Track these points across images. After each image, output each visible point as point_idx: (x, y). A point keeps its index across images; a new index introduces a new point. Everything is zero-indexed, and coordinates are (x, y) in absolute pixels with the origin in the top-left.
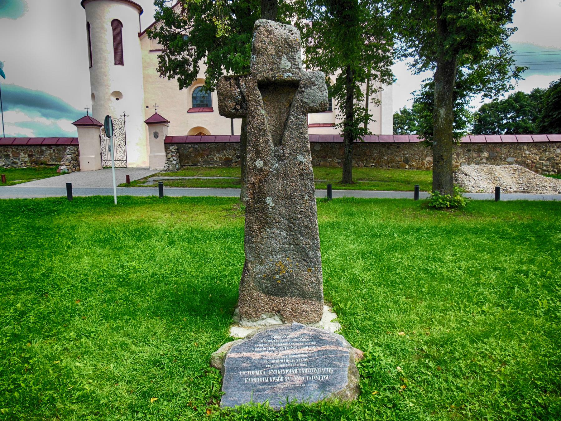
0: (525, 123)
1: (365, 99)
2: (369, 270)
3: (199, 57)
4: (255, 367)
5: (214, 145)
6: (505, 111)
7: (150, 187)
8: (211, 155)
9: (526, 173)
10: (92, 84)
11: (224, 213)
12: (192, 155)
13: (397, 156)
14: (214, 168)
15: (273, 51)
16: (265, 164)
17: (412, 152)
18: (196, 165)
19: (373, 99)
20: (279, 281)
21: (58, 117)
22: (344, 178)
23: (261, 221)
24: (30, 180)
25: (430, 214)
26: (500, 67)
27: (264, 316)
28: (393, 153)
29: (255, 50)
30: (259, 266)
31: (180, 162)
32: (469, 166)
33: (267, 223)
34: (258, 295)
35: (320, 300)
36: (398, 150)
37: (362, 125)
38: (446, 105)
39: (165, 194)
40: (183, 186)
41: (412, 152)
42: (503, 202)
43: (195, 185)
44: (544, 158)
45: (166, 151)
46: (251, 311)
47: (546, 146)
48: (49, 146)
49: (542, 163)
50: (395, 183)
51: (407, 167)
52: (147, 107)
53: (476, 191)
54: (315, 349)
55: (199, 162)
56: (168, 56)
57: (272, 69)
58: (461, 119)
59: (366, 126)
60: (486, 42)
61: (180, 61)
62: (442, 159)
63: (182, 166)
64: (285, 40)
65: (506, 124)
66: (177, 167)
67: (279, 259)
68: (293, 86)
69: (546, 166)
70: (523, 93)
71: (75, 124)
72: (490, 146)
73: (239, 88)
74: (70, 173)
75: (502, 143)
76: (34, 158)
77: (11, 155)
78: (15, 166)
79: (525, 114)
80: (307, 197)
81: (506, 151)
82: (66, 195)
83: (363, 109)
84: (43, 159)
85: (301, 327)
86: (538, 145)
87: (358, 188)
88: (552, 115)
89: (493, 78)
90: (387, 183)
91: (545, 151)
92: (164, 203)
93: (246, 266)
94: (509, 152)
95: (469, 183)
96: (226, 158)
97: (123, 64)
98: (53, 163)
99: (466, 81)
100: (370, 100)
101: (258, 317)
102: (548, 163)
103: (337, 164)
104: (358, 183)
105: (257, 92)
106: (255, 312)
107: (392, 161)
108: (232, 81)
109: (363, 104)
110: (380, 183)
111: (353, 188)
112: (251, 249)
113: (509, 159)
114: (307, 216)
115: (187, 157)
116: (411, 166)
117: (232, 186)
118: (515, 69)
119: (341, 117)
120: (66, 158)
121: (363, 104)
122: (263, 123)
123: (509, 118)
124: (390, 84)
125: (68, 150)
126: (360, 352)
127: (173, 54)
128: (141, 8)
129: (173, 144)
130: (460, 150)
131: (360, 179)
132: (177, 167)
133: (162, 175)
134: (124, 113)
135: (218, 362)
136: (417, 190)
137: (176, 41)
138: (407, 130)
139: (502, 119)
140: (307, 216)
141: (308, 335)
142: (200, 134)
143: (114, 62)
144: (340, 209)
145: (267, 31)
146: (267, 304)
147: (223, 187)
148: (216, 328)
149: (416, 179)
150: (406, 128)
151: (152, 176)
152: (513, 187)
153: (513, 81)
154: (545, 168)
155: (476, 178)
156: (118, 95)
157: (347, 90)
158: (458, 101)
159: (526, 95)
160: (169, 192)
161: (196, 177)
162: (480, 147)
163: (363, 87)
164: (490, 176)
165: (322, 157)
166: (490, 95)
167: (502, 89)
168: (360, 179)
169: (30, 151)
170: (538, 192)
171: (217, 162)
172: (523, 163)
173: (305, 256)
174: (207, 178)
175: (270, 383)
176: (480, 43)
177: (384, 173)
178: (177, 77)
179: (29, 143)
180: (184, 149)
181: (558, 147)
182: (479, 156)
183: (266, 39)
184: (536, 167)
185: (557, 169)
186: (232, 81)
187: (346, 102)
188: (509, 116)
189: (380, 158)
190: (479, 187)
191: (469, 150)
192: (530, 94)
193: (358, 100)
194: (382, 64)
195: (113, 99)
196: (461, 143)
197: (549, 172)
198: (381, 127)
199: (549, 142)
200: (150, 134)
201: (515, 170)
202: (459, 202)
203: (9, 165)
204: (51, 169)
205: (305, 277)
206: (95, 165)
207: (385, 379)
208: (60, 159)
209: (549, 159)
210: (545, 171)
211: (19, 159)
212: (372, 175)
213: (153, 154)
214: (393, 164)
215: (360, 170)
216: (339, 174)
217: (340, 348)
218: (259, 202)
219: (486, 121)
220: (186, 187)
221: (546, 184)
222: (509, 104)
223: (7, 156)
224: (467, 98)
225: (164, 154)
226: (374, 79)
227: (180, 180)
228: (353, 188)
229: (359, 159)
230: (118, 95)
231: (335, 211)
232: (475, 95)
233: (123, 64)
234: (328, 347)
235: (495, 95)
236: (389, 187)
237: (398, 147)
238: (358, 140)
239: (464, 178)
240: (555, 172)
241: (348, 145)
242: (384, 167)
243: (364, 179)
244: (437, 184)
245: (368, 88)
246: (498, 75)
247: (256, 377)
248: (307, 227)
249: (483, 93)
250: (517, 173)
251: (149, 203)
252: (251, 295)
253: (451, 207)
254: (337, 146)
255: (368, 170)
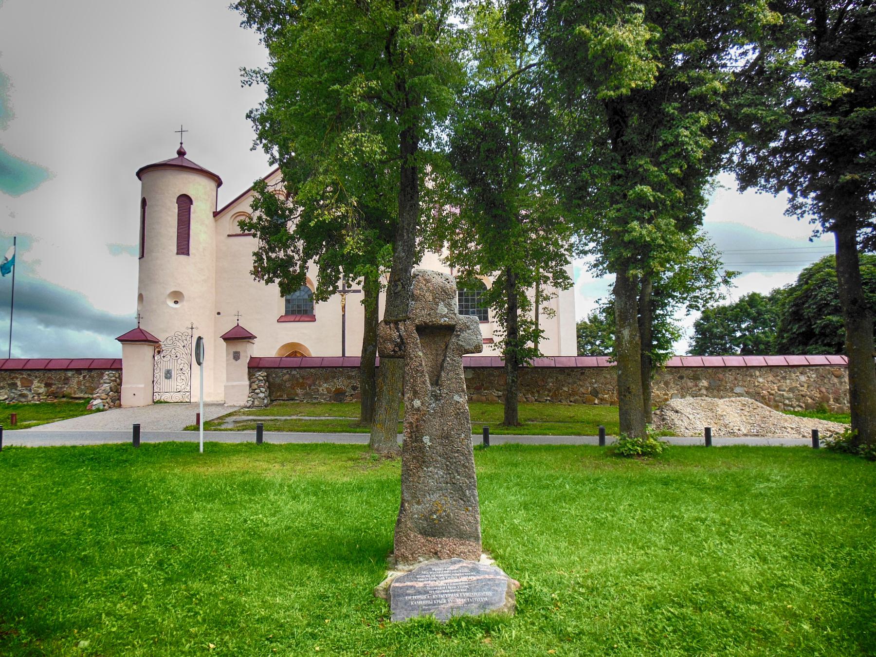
0: (767, 337)
1: (534, 309)
2: (531, 520)
3: (308, 255)
4: (420, 593)
5: (320, 371)
6: (738, 320)
7: (231, 430)
8: (315, 384)
9: (759, 409)
10: (141, 281)
11: (350, 463)
12: (288, 385)
13: (582, 386)
14: (320, 403)
15: (431, 298)
16: (422, 404)
17: (603, 380)
18: (293, 399)
19: (544, 309)
20: (436, 522)
21: (64, 325)
22: (506, 418)
23: (418, 460)
24: (48, 420)
25: (616, 464)
26: (706, 272)
27: (421, 559)
28: (575, 382)
29: (414, 297)
30: (416, 506)
31: (270, 395)
32: (682, 400)
33: (424, 462)
34: (415, 536)
35: (478, 540)
36: (582, 377)
37: (530, 344)
38: (629, 325)
39: (264, 440)
40: (279, 430)
41: (603, 380)
42: (715, 447)
43: (296, 428)
44: (784, 388)
45: (250, 379)
46: (407, 554)
47: (785, 372)
48: (78, 371)
49: (783, 395)
50: (579, 424)
51: (596, 402)
52: (219, 313)
53: (691, 434)
54: (475, 578)
55: (297, 395)
56: (267, 253)
57: (429, 314)
58: (664, 335)
59: (536, 346)
60: (660, 258)
61: (282, 259)
62: (630, 393)
63: (272, 401)
64: (442, 288)
65: (740, 337)
66: (266, 401)
67: (437, 501)
68: (450, 329)
69: (788, 399)
70: (759, 295)
71: (120, 339)
72: (710, 371)
73: (398, 331)
74: (106, 410)
75: (726, 367)
76: (54, 388)
77: (19, 383)
78: (23, 400)
79: (764, 324)
80: (463, 435)
81: (732, 378)
82: (132, 441)
83: (531, 323)
84: (66, 390)
85: (460, 561)
86: (775, 370)
87: (527, 431)
88: (792, 328)
89: (698, 284)
90: (567, 425)
91: (784, 378)
92: (266, 452)
93: (402, 505)
94: (736, 379)
95: (681, 423)
96: (337, 390)
97: (188, 254)
98: (82, 395)
99: (666, 286)
100: (541, 311)
101: (415, 559)
102: (791, 395)
103: (497, 399)
104: (527, 425)
105: (416, 335)
106: (412, 554)
107: (574, 393)
108: (392, 325)
109: (530, 316)
110: (557, 424)
111: (519, 432)
112: (408, 488)
113: (738, 390)
114: (463, 455)
115: (280, 387)
116: (602, 400)
117: (348, 429)
118: (724, 274)
119: (501, 333)
120: (103, 388)
121: (530, 316)
122: (421, 365)
123: (745, 329)
124: (566, 288)
125: (106, 377)
126: (517, 582)
127: (273, 251)
128: (219, 179)
129: (260, 369)
130: (668, 377)
131: (529, 420)
132: (266, 401)
133: (244, 414)
134: (192, 324)
135: (382, 593)
136: (602, 434)
137: (279, 235)
138: (599, 346)
139: (735, 331)
140: (463, 455)
141: (467, 567)
142: (294, 354)
143: (175, 251)
144: (500, 458)
145: (425, 280)
146: (424, 546)
147: (335, 432)
148: (372, 572)
149: (608, 418)
150: (598, 343)
151: (230, 415)
152: (742, 429)
153: (723, 289)
154: (787, 402)
155: (691, 417)
156: (177, 297)
157: (509, 299)
158: (658, 312)
159: (763, 298)
160: (270, 437)
161: (294, 417)
162: (695, 373)
163: (530, 293)
164: (710, 414)
165: (475, 388)
166: (696, 306)
167: (710, 298)
168: (529, 420)
169: (49, 378)
170: (776, 435)
171: (324, 395)
172: (757, 396)
173: (461, 494)
174: (312, 418)
175: (434, 605)
176: (654, 258)
177: (564, 411)
178: (277, 280)
179: (49, 367)
180: (277, 376)
181: (801, 373)
182: (697, 386)
183: (424, 287)
184: (775, 401)
185: (804, 403)
186: (392, 325)
187: (507, 314)
188: (743, 326)
189: (558, 389)
190: (695, 429)
191: (681, 378)
192: (769, 296)
193: (523, 310)
194: (554, 263)
195: (171, 303)
196: (666, 367)
197: (794, 407)
198: (558, 343)
199: (789, 366)
200: (228, 355)
201: (744, 405)
202: (653, 447)
203: (14, 398)
204: (77, 404)
205: (463, 516)
206: (143, 399)
207: (540, 601)
208: (92, 390)
209: (791, 390)
210: (789, 405)
211: (30, 390)
212: (547, 413)
213: (230, 384)
214: (577, 397)
215: (529, 407)
216: (499, 412)
217: (498, 577)
218: (416, 441)
219: (712, 333)
220: (283, 431)
221: (786, 425)
222: (741, 310)
223: (14, 386)
224: (669, 309)
225: (248, 383)
226: (545, 282)
227: (272, 420)
228: (519, 432)
229: (528, 391)
230: (177, 297)
231: (494, 461)
232: (680, 305)
233: (188, 254)
234: (487, 576)
235: (703, 306)
236: (570, 430)
237: (582, 374)
238: (525, 364)
239: (674, 416)
240: (801, 407)
241: (512, 372)
242: (564, 403)
243: (535, 419)
244: (625, 425)
245: (539, 294)
246: (704, 280)
247: (422, 600)
248: (463, 465)
249: (687, 303)
250: (747, 409)
251: (246, 452)
252: (407, 536)
253: (644, 454)
254: (496, 373)
255: (541, 405)
